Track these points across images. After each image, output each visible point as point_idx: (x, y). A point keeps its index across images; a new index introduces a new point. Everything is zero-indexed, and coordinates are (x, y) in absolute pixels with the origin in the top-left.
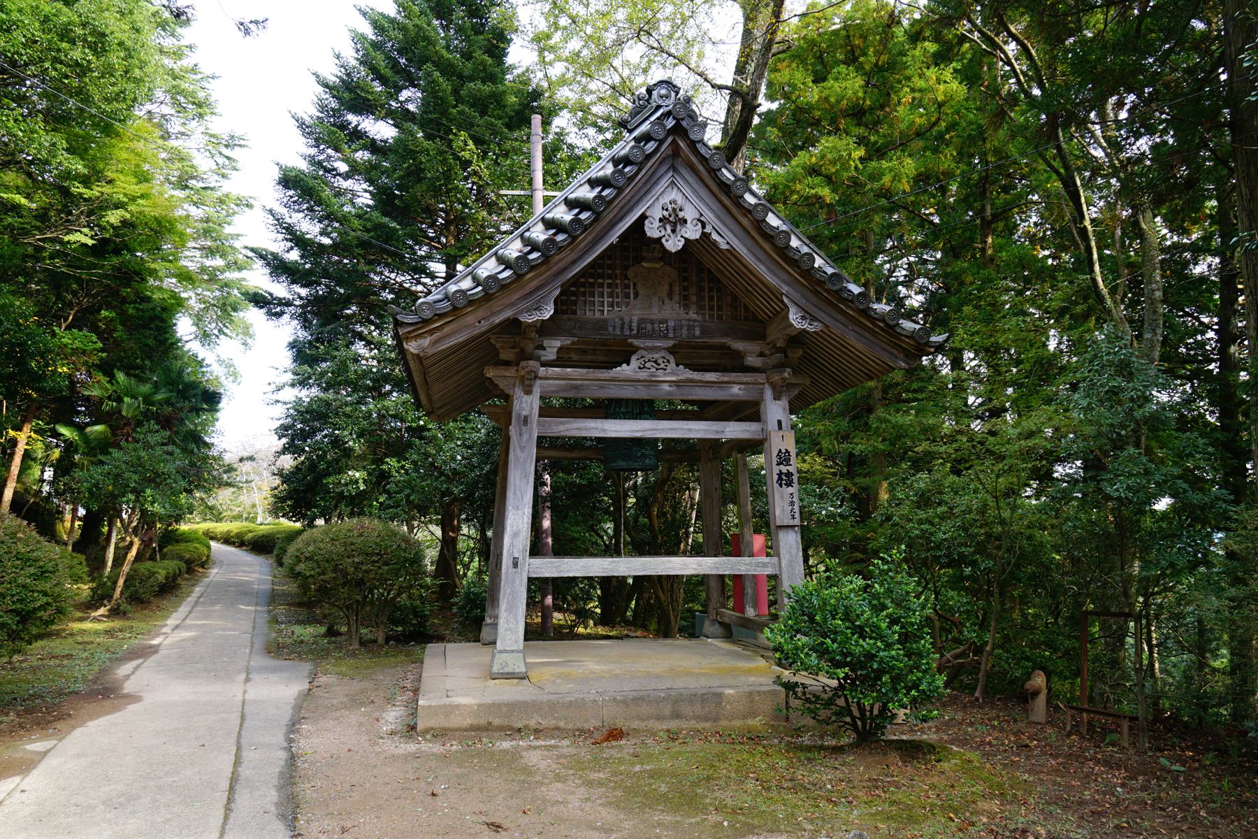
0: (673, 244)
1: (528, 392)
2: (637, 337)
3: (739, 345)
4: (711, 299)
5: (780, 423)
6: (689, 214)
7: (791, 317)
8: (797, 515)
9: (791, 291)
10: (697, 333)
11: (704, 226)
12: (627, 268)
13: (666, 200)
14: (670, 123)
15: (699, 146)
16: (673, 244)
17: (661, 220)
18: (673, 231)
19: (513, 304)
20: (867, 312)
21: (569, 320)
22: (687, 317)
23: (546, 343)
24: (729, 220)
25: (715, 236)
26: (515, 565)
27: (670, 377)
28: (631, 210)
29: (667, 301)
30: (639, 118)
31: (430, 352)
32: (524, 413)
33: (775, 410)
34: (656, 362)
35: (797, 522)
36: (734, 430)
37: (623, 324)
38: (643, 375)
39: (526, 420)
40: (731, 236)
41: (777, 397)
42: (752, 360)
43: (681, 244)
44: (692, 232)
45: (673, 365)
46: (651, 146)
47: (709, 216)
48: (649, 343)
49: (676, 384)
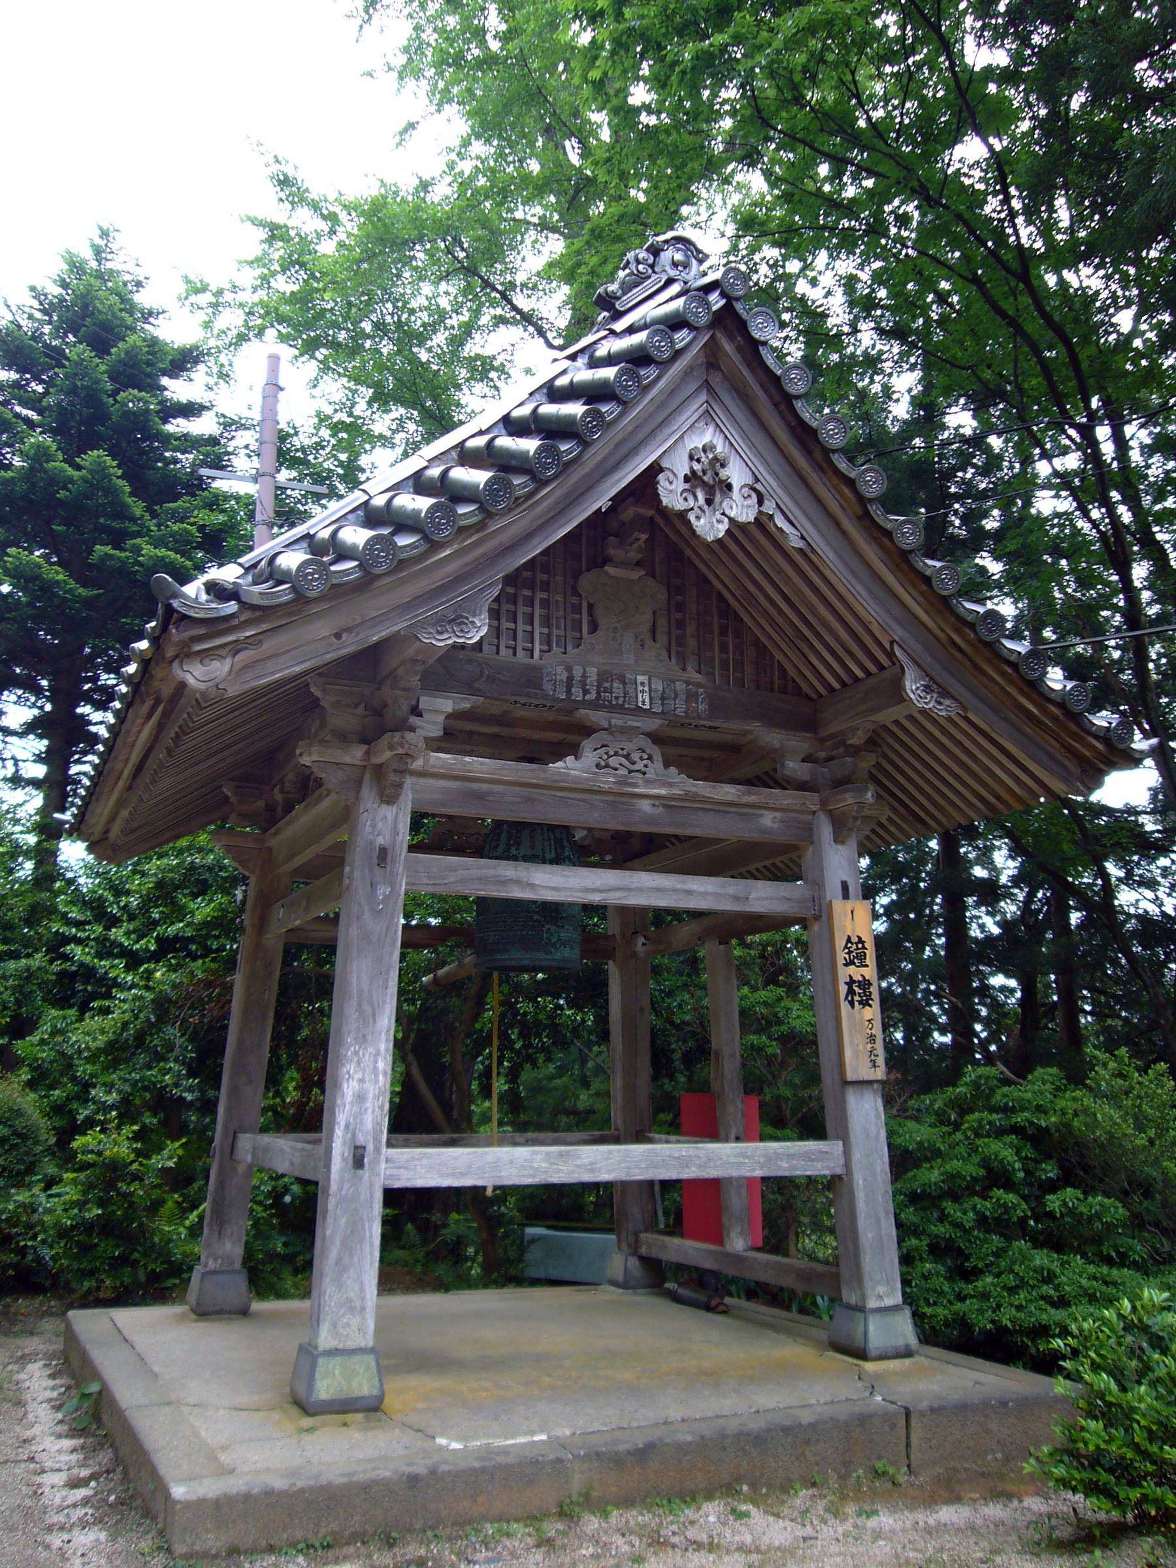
0: (710, 527)
1: (389, 797)
2: (595, 705)
3: (772, 738)
4: (724, 648)
5: (845, 886)
6: (736, 474)
7: (908, 684)
8: (881, 1061)
9: (907, 636)
10: (702, 707)
11: (760, 502)
12: (577, 574)
13: (697, 441)
14: (716, 301)
15: (763, 351)
16: (710, 527)
17: (687, 479)
18: (709, 502)
19: (408, 606)
20: (1036, 686)
21: (470, 661)
22: (685, 676)
23: (425, 702)
24: (802, 495)
25: (780, 522)
26: (358, 1160)
27: (654, 790)
28: (633, 452)
29: (649, 642)
30: (638, 294)
31: (233, 690)
32: (380, 840)
33: (843, 863)
34: (627, 757)
35: (880, 1073)
36: (763, 897)
37: (570, 679)
38: (607, 781)
39: (383, 855)
40: (808, 525)
41: (838, 839)
42: (794, 767)
43: (721, 529)
44: (741, 509)
45: (658, 764)
46: (682, 337)
47: (769, 482)
48: (617, 720)
49: (667, 803)
